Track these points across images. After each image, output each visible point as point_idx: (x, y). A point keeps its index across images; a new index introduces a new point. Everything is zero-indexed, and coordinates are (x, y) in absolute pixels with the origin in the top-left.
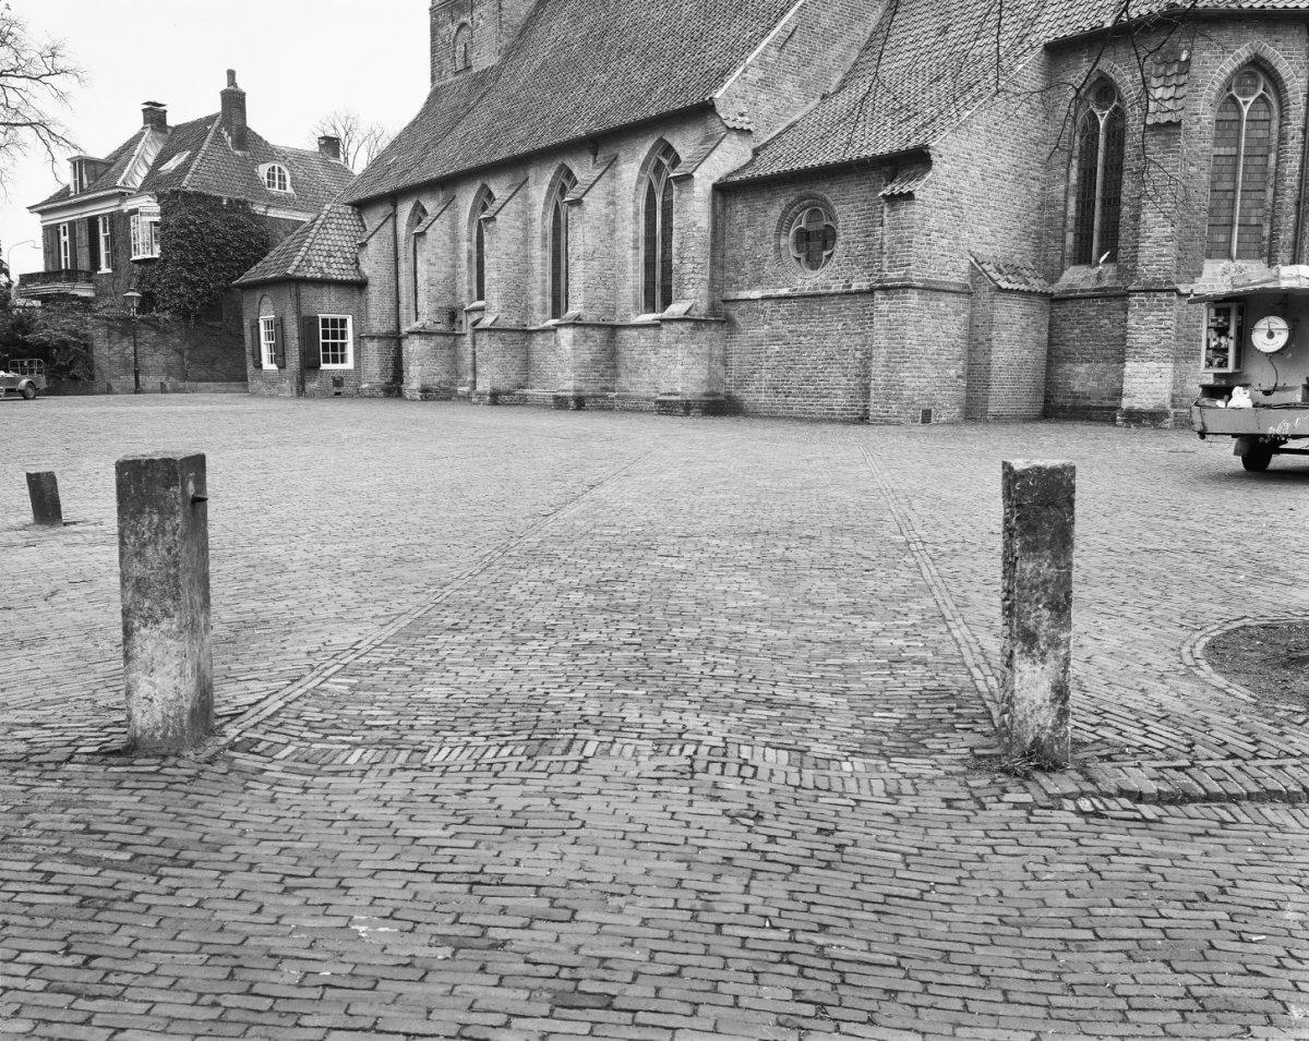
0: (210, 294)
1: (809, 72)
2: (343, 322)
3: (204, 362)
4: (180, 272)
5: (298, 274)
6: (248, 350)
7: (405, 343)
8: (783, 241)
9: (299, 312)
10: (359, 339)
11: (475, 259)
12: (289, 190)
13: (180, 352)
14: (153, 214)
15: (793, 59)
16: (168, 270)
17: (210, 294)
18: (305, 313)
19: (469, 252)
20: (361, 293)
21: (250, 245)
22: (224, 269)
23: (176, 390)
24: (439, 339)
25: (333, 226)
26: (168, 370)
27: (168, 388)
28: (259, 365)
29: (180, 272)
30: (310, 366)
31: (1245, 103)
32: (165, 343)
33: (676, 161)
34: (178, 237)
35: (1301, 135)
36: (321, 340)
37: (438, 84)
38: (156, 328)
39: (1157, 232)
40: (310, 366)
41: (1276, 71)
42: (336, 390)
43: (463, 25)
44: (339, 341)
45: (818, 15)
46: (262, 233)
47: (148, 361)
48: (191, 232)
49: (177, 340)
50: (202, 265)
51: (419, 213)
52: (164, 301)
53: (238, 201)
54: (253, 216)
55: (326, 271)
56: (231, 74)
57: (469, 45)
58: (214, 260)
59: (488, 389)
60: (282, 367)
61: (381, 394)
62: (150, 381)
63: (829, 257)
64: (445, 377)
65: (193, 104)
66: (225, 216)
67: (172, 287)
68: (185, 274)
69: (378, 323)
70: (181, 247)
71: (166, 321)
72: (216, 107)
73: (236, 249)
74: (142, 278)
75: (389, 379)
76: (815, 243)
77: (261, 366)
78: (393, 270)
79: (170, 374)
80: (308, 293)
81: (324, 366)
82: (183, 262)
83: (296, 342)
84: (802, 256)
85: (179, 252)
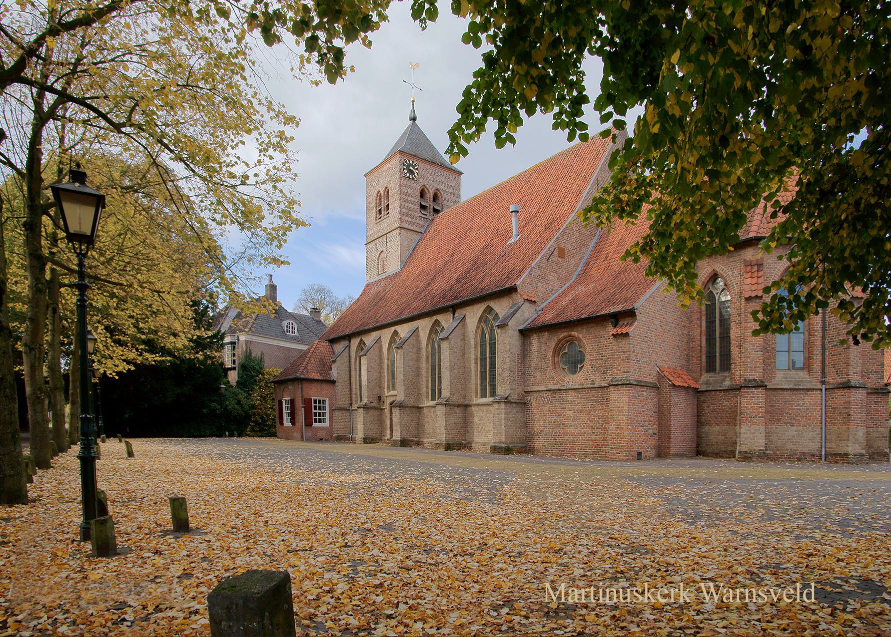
72: (262, 292)
81: (315, 425)
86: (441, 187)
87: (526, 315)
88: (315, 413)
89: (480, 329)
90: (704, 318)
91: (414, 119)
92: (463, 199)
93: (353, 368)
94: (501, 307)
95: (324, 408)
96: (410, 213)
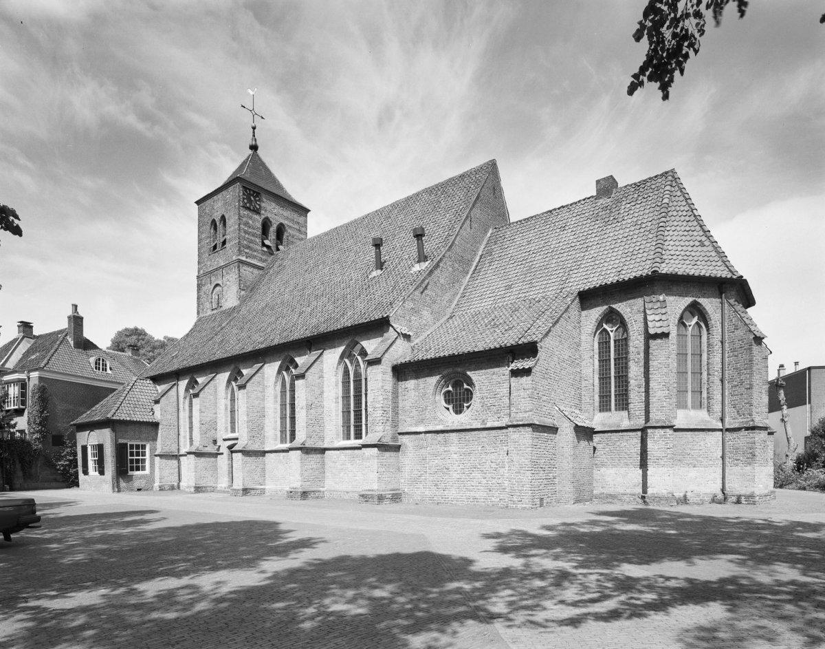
1: (436, 307)
5: (114, 418)
8: (437, 398)
11: (229, 409)
15: (428, 298)
25: (137, 390)
31: (690, 326)
33: (296, 366)
35: (720, 344)
36: (129, 458)
37: (201, 315)
39: (659, 394)
41: (705, 309)
43: (217, 285)
44: (141, 457)
45: (439, 277)
51: (193, 384)
56: (75, 307)
57: (220, 296)
59: (241, 487)
63: (468, 407)
65: (50, 322)
72: (63, 324)
76: (459, 398)
84: (450, 407)
86: (286, 222)
87: (401, 352)
88: (132, 461)
89: (230, 389)
90: (597, 356)
91: (254, 148)
92: (309, 236)
93: (181, 409)
94: (371, 345)
95: (144, 454)
96: (251, 245)
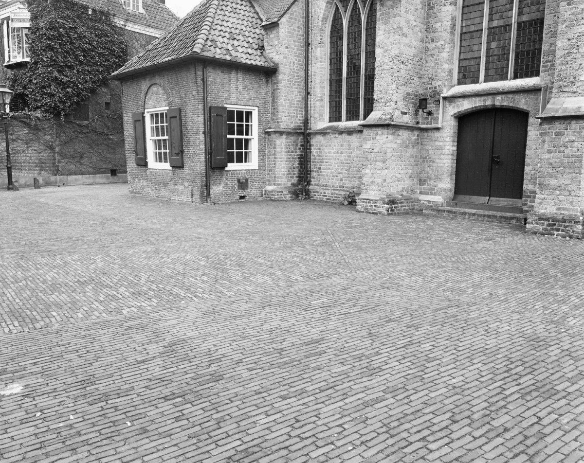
0: (78, 95)
2: (249, 114)
3: (73, 157)
4: (51, 73)
6: (129, 144)
7: (316, 141)
9: (204, 102)
10: (266, 134)
12: (141, 10)
13: (52, 148)
14: (24, 20)
16: (40, 71)
17: (78, 95)
18: (211, 102)
19: (453, 19)
20: (267, 82)
21: (112, 52)
22: (90, 72)
23: (48, 184)
24: (405, 134)
25: (229, 9)
26: (41, 166)
27: (41, 181)
28: (143, 163)
29: (51, 73)
30: (216, 165)
32: (38, 139)
34: (48, 39)
38: (28, 125)
40: (216, 165)
42: (241, 193)
46: (122, 43)
47: (21, 157)
48: (60, 35)
49: (48, 137)
50: (71, 67)
52: (35, 100)
53: (102, 12)
54: (114, 27)
55: (233, 53)
58: (81, 63)
60: (178, 166)
61: (288, 197)
62: (22, 176)
64: (408, 183)
66: (91, 24)
67: (44, 87)
68: (56, 74)
69: (288, 116)
70: (52, 49)
71: (38, 118)
73: (101, 55)
74: (15, 81)
75: (295, 180)
77: (145, 165)
78: (302, 57)
79: (42, 169)
80: (215, 77)
82: (53, 63)
83: (202, 137)
85: (50, 54)
